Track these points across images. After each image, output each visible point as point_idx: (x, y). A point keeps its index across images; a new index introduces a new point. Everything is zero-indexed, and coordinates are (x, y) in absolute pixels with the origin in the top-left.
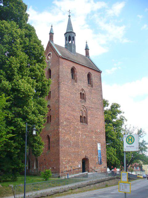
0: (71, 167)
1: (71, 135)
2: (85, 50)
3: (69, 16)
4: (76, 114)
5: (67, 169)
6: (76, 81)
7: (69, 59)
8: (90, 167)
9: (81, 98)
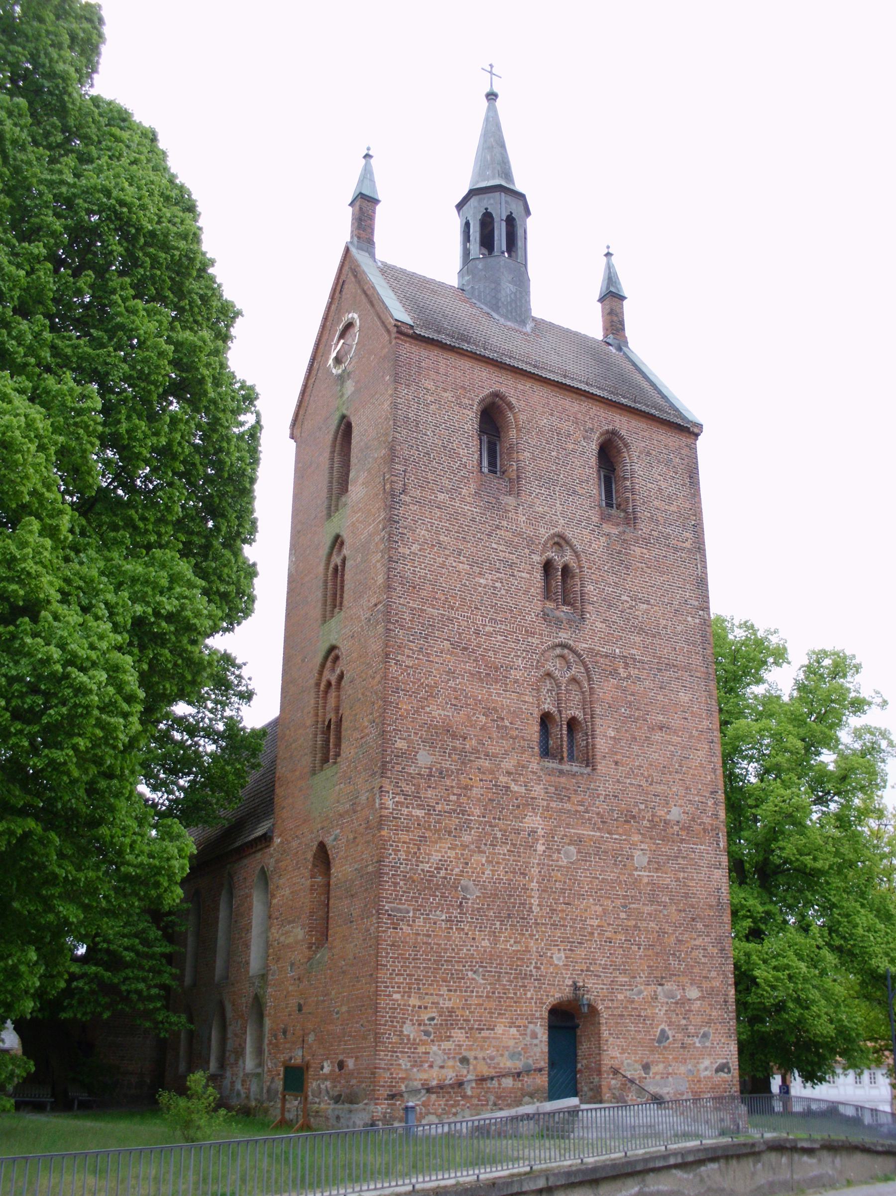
0: (464, 1060)
1: (466, 838)
2: (601, 300)
3: (492, 96)
4: (504, 699)
5: (434, 1077)
6: (514, 486)
7: (465, 346)
8: (607, 1062)
9: (548, 593)
